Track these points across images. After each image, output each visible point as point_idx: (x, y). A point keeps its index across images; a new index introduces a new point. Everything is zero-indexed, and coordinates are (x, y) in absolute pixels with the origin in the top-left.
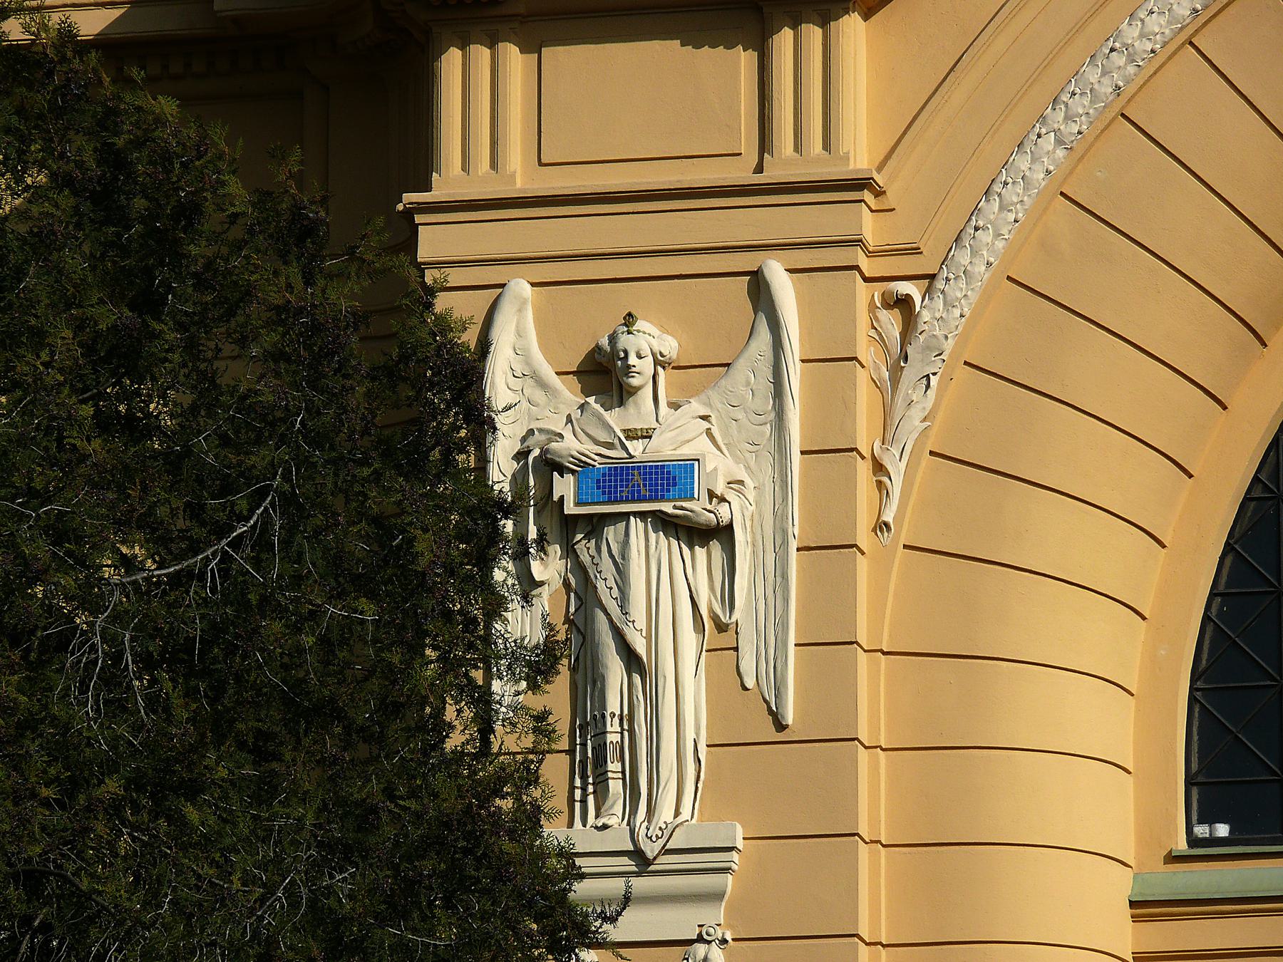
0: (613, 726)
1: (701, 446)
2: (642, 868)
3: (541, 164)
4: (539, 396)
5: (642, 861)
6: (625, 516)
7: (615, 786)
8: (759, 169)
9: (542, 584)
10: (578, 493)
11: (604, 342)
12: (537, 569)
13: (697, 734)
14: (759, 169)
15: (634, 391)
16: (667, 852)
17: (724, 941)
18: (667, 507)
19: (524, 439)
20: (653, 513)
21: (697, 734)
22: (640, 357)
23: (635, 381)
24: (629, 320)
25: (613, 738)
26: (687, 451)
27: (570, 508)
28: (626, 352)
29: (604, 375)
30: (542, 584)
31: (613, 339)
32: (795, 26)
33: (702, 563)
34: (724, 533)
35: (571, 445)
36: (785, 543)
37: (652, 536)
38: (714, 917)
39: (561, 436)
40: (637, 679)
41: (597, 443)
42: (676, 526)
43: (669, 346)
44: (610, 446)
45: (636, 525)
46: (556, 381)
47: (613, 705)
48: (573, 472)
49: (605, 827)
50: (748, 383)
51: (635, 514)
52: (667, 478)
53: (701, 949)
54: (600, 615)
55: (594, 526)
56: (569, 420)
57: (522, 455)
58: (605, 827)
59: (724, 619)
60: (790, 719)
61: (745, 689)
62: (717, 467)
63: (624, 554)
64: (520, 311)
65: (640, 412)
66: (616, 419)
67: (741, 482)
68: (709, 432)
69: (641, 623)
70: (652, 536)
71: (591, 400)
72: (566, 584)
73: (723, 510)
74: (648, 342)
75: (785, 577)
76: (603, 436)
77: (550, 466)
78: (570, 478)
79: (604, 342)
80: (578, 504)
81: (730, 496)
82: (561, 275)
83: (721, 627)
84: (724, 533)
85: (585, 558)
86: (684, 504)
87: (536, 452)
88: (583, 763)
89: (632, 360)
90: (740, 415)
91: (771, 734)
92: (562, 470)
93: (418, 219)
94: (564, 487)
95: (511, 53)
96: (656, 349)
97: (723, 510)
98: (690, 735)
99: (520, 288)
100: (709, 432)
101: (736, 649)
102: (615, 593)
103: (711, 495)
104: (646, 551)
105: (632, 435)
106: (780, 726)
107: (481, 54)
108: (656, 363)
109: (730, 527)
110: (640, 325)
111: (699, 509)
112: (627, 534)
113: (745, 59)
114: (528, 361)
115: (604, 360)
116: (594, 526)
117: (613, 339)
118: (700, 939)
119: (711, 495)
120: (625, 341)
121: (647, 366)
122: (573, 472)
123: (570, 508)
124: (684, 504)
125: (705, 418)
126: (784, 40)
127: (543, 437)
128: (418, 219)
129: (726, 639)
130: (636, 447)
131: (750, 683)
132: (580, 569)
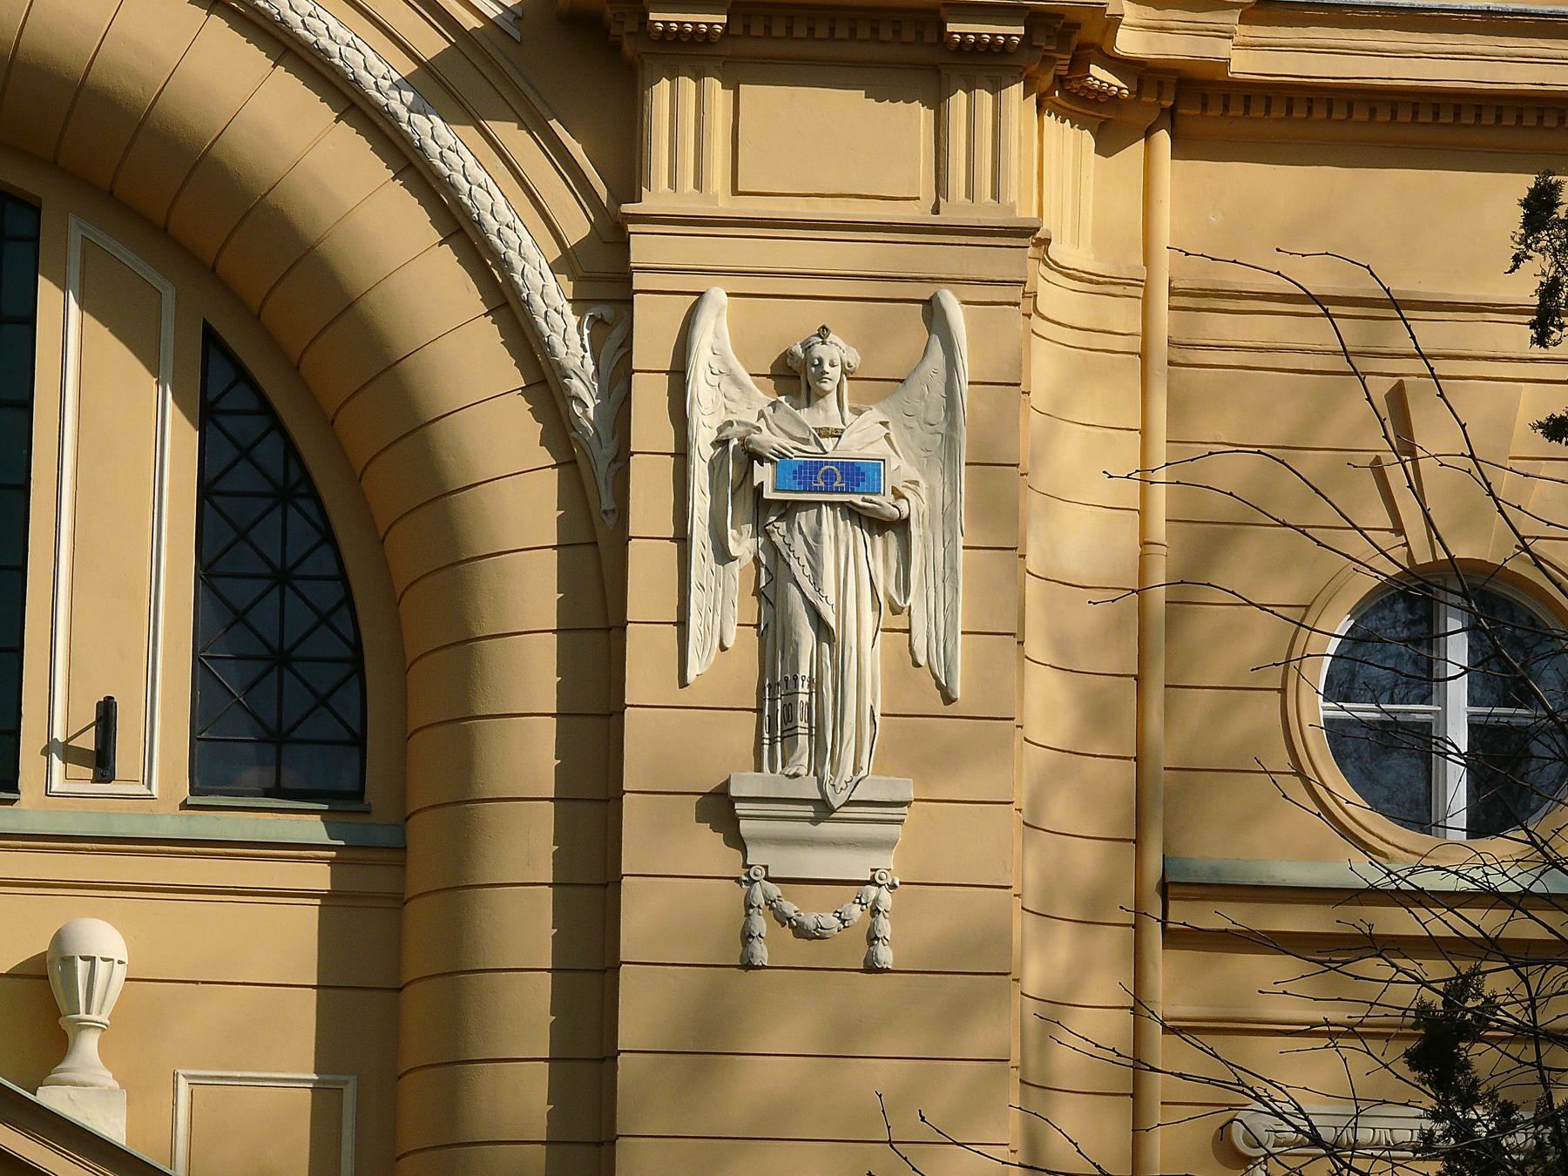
0: (803, 688)
1: (880, 449)
2: (820, 815)
3: (735, 192)
4: (734, 392)
5: (823, 809)
6: (819, 503)
7: (803, 740)
8: (936, 211)
9: (734, 559)
10: (776, 477)
11: (798, 350)
12: (733, 548)
13: (874, 701)
14: (936, 211)
15: (823, 394)
16: (849, 803)
17: (894, 886)
18: (857, 499)
19: (720, 430)
20: (842, 503)
21: (874, 701)
22: (832, 365)
23: (827, 386)
24: (823, 332)
25: (803, 698)
26: (872, 452)
27: (768, 494)
28: (820, 360)
29: (794, 377)
30: (734, 559)
31: (807, 347)
32: (969, 89)
33: (877, 555)
34: (901, 526)
35: (769, 439)
36: (954, 539)
37: (841, 523)
38: (885, 862)
39: (759, 429)
40: (826, 646)
41: (792, 438)
42: (859, 516)
43: (853, 357)
44: (806, 442)
45: (827, 513)
46: (748, 380)
47: (804, 671)
48: (772, 461)
49: (796, 776)
50: (923, 396)
51: (826, 503)
52: (855, 474)
53: (872, 891)
54: (793, 589)
55: (787, 510)
56: (761, 415)
57: (721, 443)
58: (796, 776)
59: (900, 603)
60: (958, 694)
61: (916, 664)
62: (900, 467)
63: (817, 536)
64: (718, 315)
65: (825, 414)
66: (812, 417)
67: (916, 483)
68: (887, 437)
69: (832, 600)
70: (841, 523)
71: (782, 399)
72: (756, 560)
73: (903, 504)
74: (836, 353)
75: (954, 569)
76: (799, 433)
77: (751, 455)
78: (767, 465)
79: (798, 350)
80: (776, 490)
81: (908, 494)
82: (754, 287)
83: (895, 610)
84: (901, 526)
85: (777, 539)
86: (874, 498)
87: (735, 442)
88: (773, 718)
89: (827, 368)
90: (914, 424)
91: (938, 706)
92: (762, 459)
93: (631, 228)
94: (763, 474)
95: (715, 88)
96: (845, 360)
97: (903, 504)
98: (869, 702)
99: (718, 294)
100: (887, 437)
101: (909, 631)
102: (808, 571)
103: (894, 491)
104: (838, 538)
105: (824, 433)
106: (948, 699)
107: (688, 85)
108: (844, 372)
109: (908, 520)
110: (832, 337)
111: (884, 502)
112: (819, 522)
113: (923, 115)
114: (724, 361)
115: (795, 366)
116: (787, 510)
117: (807, 347)
118: (872, 882)
119: (894, 491)
120: (819, 350)
121: (834, 373)
122: (772, 461)
123: (768, 494)
124: (874, 498)
125: (884, 424)
126: (959, 100)
127: (742, 429)
128: (631, 228)
129: (900, 622)
130: (828, 443)
131: (922, 660)
132: (773, 550)
